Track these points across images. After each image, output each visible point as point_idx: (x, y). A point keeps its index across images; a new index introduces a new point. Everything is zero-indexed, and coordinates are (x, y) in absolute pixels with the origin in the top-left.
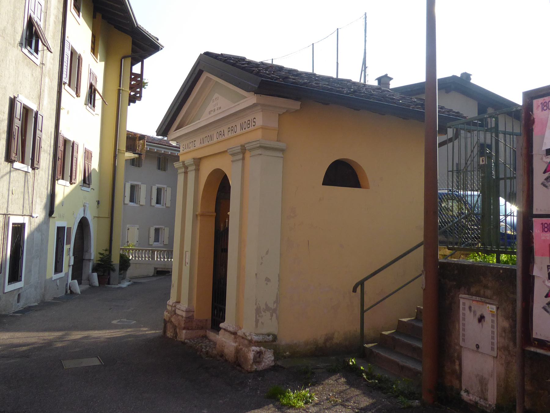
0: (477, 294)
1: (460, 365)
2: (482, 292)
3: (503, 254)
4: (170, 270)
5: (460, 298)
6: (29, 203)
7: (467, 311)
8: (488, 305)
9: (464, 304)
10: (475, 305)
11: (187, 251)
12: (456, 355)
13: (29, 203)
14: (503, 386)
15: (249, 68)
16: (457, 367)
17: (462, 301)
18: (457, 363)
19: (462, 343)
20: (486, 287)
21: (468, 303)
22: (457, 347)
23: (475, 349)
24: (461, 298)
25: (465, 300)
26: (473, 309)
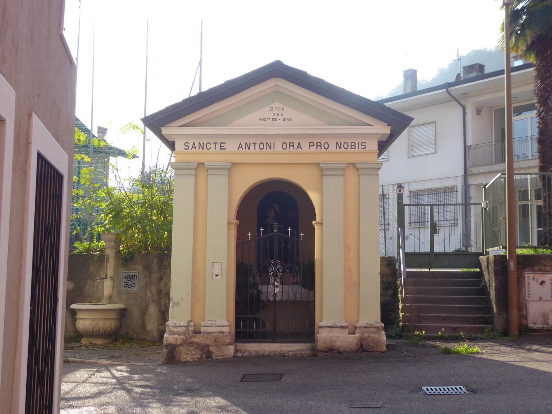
0: (539, 270)
1: (526, 311)
2: (543, 268)
3: (494, 260)
4: (65, 351)
5: (525, 274)
6: (503, 357)
7: (531, 281)
8: (547, 275)
9: (528, 277)
10: (537, 276)
11: (435, 154)
12: (524, 306)
13: (503, 357)
14: (88, 333)
15: (77, 359)
16: (524, 313)
17: (527, 276)
18: (525, 310)
19: (527, 299)
20: (545, 266)
21: (531, 276)
22: (524, 302)
23: (538, 299)
24: (526, 274)
25: (529, 274)
26: (535, 279)
